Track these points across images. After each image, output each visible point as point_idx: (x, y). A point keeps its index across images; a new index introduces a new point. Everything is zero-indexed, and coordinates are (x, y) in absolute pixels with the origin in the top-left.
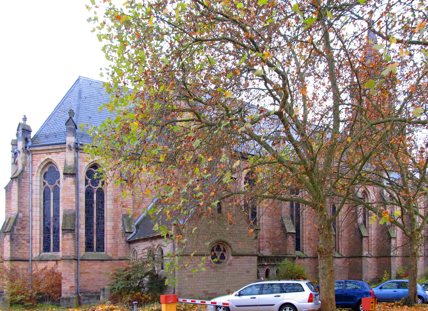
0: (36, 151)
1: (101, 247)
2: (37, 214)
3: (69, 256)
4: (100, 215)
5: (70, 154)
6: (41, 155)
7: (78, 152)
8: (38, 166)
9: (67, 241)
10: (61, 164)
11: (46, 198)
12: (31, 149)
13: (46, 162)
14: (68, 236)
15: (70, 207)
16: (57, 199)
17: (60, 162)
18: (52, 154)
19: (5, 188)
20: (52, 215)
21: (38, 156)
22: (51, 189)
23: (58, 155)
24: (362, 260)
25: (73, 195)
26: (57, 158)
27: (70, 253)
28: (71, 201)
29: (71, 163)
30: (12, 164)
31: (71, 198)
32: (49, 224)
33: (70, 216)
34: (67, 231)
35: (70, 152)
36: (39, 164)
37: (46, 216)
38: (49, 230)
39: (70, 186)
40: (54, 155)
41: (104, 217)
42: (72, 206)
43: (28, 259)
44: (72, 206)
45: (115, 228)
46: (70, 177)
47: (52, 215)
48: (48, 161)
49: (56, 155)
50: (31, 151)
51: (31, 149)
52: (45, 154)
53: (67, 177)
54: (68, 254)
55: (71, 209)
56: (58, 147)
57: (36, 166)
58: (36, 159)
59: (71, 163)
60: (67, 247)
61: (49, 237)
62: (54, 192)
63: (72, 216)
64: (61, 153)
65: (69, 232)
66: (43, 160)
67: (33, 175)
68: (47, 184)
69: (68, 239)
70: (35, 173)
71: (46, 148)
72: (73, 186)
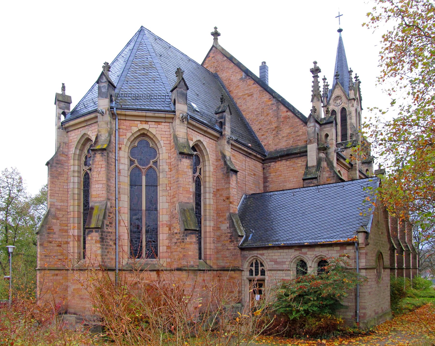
0: (125, 115)
1: (153, 253)
2: (124, 203)
3: (193, 266)
4: (198, 211)
5: (182, 127)
6: (133, 122)
7: (115, 119)
8: (128, 137)
9: (190, 246)
10: (163, 139)
11: (134, 184)
12: (119, 112)
13: (139, 133)
14: (191, 238)
15: (186, 199)
16: (153, 185)
17: (162, 136)
18: (149, 123)
19: (48, 164)
20: (144, 208)
21: (127, 123)
22: (143, 171)
23: (159, 126)
24: (66, 278)
25: (190, 183)
26: (157, 129)
27: (194, 262)
28: (188, 191)
29: (183, 140)
30: (59, 128)
31: (187, 186)
32: (140, 219)
33: (189, 211)
34: (190, 232)
35: (182, 124)
36: (129, 135)
37: (134, 210)
38: (139, 227)
39: (186, 170)
40: (152, 125)
41: (201, 214)
42: (189, 198)
43: (114, 268)
44: (189, 198)
45: (217, 228)
46: (186, 158)
47: (144, 208)
48: (142, 132)
49: (156, 126)
50: (118, 114)
51: (119, 112)
52: (139, 122)
53: (183, 158)
54: (192, 263)
55: (188, 201)
56: (162, 115)
57: (125, 137)
58: (125, 127)
59: (183, 140)
60: (190, 253)
61: (139, 239)
62: (147, 175)
63: (191, 211)
64: (163, 124)
65: (192, 234)
66: (135, 129)
67: (120, 148)
68: (136, 163)
69: (191, 243)
70: (123, 147)
71: (144, 113)
72: (190, 170)
